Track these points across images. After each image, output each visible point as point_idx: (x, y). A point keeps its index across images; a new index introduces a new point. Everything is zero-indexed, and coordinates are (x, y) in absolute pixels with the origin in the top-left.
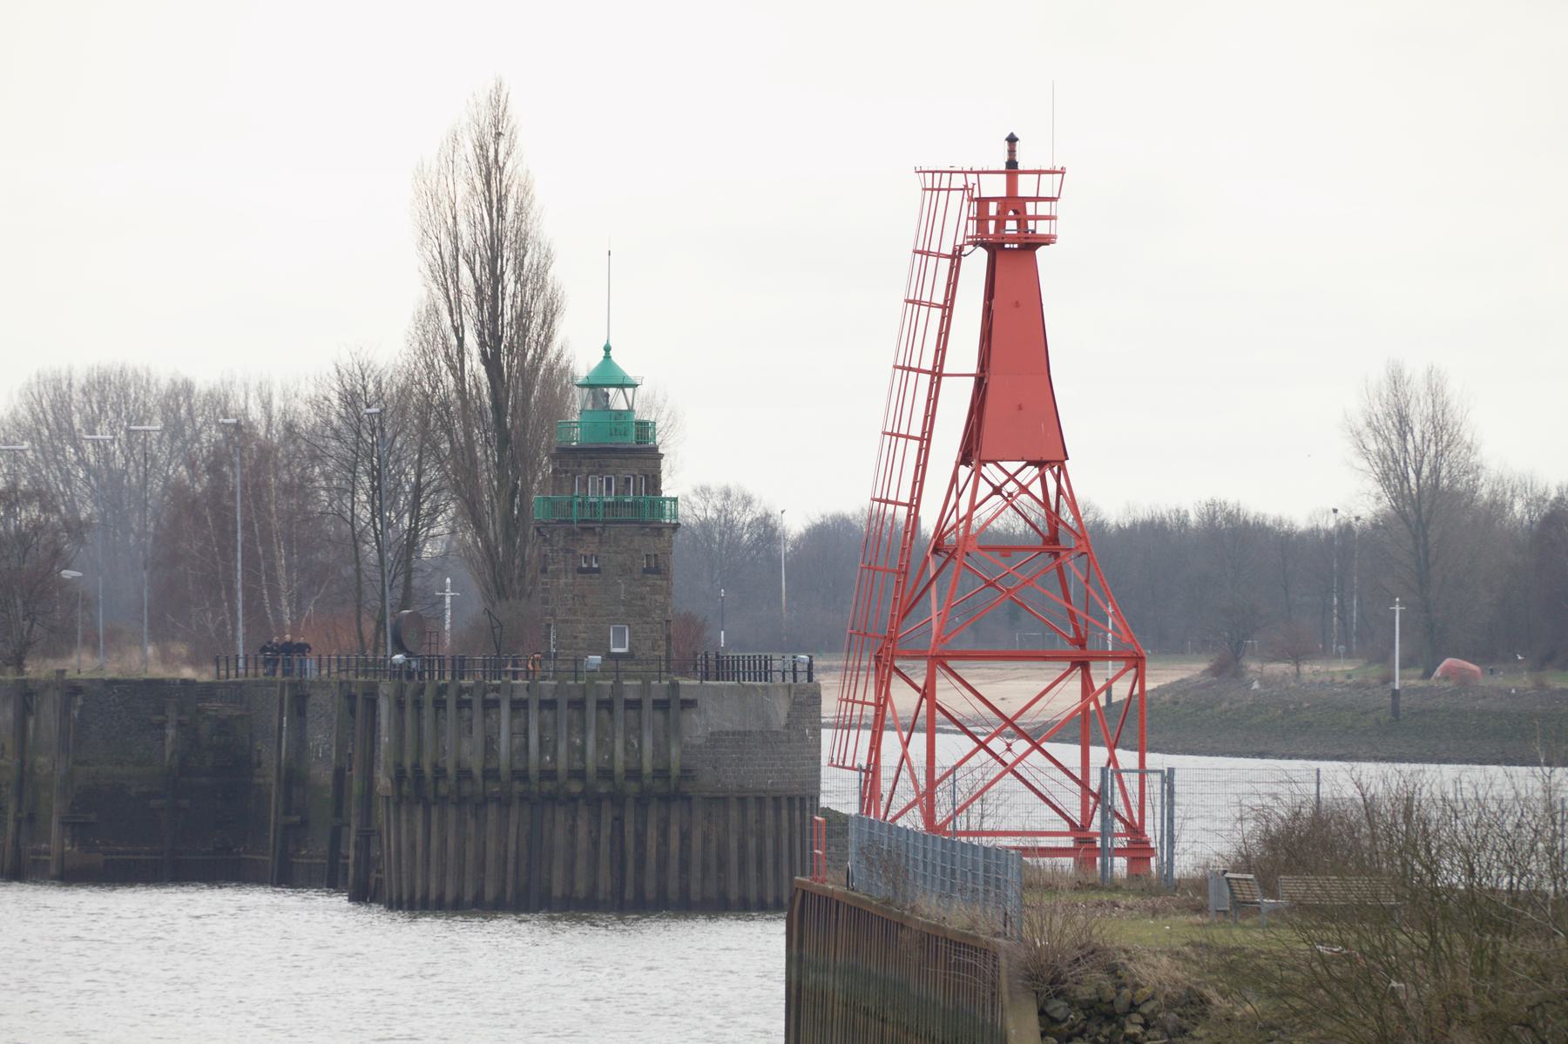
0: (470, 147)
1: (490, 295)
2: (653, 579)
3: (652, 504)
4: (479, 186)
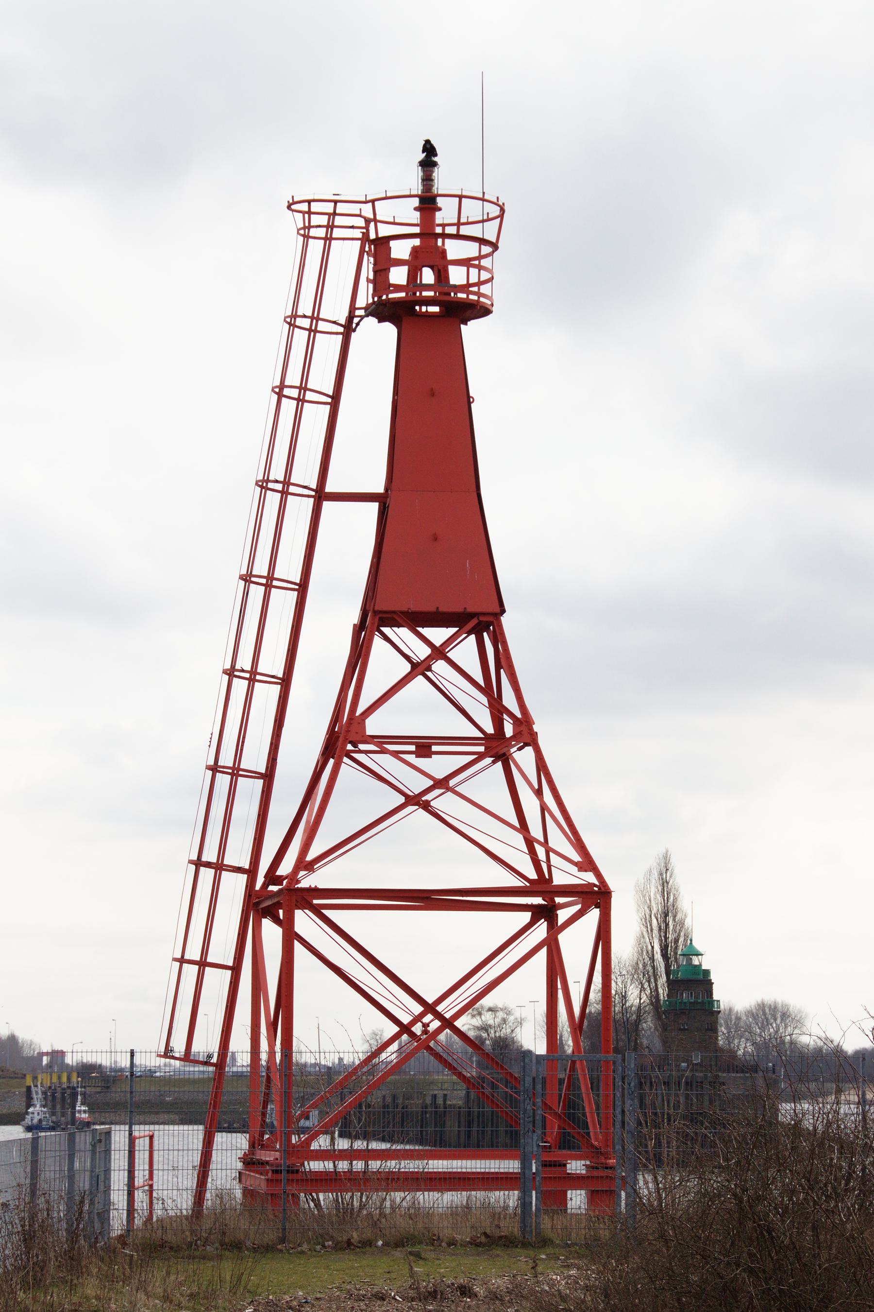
0: (656, 874)
1: (664, 929)
2: (709, 1033)
3: (709, 1003)
4: (660, 888)
